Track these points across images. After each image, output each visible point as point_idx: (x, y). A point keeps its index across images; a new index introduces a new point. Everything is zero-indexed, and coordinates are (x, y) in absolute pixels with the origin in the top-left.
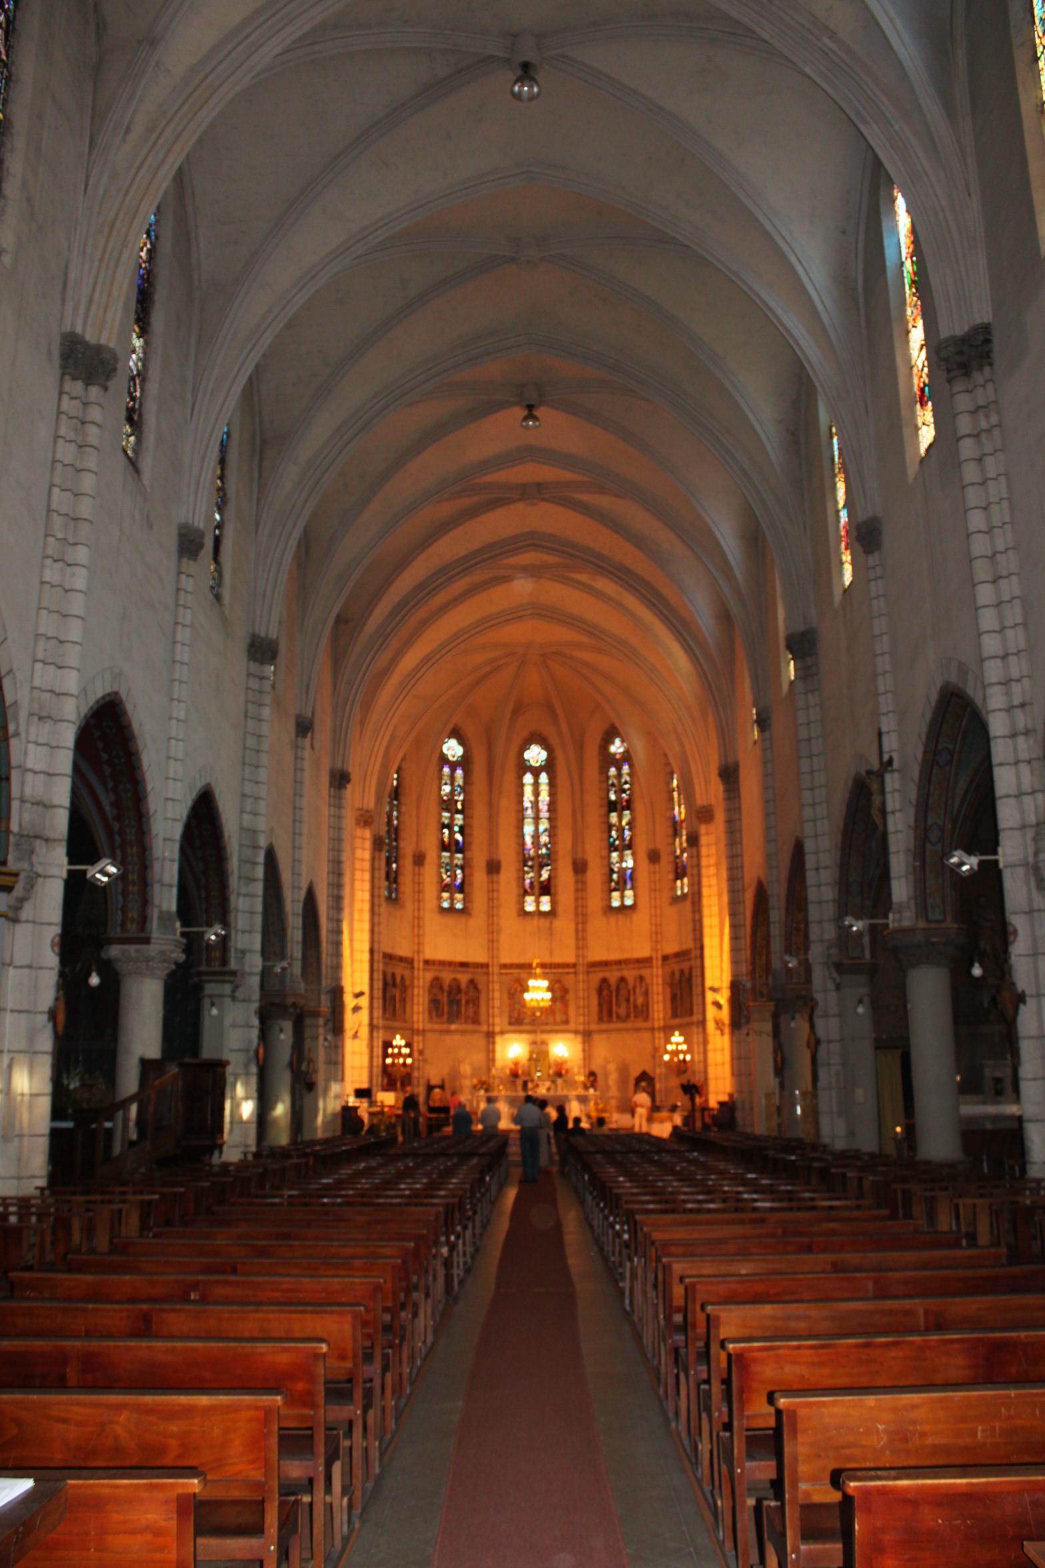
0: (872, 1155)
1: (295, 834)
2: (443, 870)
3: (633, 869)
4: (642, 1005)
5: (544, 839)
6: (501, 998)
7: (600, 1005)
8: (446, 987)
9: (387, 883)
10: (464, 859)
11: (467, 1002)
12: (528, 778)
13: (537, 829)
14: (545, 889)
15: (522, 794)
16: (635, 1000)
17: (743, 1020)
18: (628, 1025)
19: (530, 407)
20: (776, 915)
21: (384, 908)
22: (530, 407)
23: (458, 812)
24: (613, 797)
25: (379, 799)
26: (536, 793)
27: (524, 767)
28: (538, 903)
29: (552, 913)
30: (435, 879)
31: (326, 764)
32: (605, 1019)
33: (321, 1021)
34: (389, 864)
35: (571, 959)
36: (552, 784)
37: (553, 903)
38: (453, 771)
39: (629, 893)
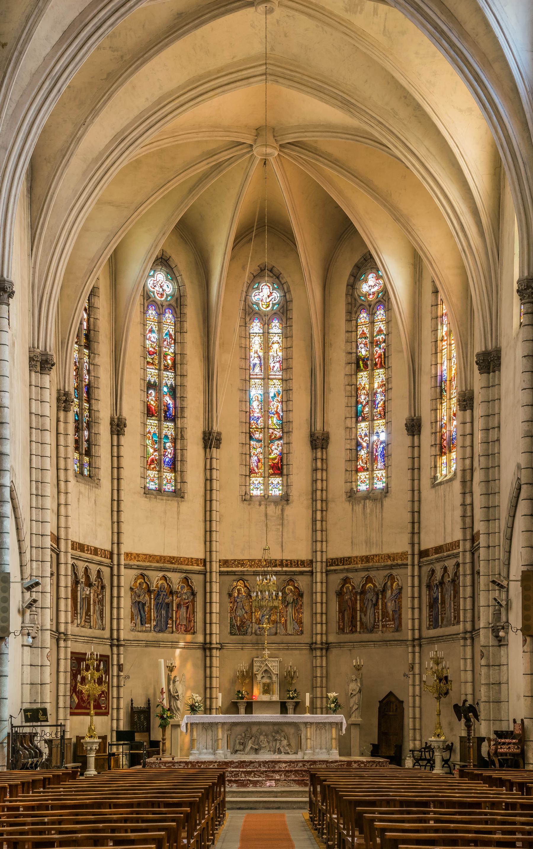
2: (149, 442)
3: (387, 444)
4: (164, 314)
5: (275, 405)
6: (220, 603)
7: (341, 611)
9: (77, 455)
10: (176, 428)
11: (179, 606)
12: (256, 327)
14: (278, 469)
18: (376, 636)
21: (73, 486)
23: (166, 368)
24: (363, 352)
26: (266, 346)
27: (250, 312)
28: (266, 485)
29: (286, 499)
30: (138, 452)
32: (347, 630)
35: (304, 554)
36: (287, 335)
37: (287, 486)
38: (160, 315)
39: (380, 473)
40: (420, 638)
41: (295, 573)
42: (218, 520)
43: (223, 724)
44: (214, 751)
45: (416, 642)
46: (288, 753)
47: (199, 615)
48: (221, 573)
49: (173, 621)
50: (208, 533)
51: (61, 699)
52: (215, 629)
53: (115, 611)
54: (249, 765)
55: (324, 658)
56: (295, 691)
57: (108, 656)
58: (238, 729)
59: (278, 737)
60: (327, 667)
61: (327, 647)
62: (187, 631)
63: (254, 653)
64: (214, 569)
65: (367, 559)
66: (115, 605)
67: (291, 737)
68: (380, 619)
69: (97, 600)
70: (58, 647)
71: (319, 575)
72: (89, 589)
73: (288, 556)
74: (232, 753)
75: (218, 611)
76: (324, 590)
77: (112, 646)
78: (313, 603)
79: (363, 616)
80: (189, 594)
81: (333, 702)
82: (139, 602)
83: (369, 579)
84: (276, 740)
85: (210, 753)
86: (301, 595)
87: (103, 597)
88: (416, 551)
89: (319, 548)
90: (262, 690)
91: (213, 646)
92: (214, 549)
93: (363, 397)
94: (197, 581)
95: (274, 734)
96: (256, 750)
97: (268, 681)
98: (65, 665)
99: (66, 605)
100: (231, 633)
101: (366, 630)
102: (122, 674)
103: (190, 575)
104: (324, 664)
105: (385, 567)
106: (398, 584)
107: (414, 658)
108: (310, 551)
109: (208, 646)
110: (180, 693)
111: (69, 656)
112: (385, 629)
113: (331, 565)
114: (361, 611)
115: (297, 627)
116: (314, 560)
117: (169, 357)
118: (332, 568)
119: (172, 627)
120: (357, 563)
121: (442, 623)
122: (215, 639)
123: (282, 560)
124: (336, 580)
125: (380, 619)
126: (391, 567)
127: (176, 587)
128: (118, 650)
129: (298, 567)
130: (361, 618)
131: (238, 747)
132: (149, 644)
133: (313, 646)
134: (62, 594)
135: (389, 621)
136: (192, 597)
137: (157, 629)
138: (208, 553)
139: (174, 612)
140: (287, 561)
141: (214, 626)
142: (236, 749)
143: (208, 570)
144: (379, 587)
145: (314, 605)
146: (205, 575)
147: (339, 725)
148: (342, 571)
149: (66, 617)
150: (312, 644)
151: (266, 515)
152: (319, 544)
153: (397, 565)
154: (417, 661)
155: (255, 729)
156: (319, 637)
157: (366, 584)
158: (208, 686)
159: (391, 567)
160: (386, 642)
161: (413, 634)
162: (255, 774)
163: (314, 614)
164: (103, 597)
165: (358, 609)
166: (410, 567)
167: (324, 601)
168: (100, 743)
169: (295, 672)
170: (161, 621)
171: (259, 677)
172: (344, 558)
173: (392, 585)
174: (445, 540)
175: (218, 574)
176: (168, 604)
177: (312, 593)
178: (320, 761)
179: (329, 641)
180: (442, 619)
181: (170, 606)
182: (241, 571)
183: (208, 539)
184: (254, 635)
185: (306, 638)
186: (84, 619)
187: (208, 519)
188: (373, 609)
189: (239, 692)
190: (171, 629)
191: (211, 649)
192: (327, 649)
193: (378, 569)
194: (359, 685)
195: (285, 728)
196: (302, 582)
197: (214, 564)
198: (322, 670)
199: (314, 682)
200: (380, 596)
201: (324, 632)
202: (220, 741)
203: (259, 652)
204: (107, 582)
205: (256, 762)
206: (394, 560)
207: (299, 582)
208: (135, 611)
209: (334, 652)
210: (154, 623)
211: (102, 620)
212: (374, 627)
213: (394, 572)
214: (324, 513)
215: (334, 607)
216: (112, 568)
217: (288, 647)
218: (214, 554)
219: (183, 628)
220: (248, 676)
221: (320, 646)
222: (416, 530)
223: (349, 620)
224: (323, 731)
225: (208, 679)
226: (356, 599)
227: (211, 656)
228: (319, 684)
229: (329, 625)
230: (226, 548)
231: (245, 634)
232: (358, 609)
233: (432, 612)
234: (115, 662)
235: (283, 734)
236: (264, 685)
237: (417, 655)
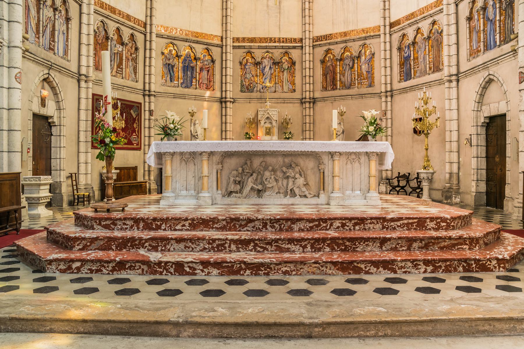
7: (325, 75)
11: (201, 69)
18: (353, 91)
35: (297, 35)
40: (391, 91)
41: (289, 48)
42: (232, 8)
43: (211, 154)
44: (198, 193)
45: (389, 94)
46: (305, 196)
47: (217, 77)
48: (234, 47)
49: (196, 80)
50: (224, 17)
51: (82, 134)
52: (229, 87)
53: (147, 68)
54: (246, 225)
55: (312, 109)
56: (290, 133)
57: (140, 104)
58: (233, 162)
59: (290, 173)
60: (313, 116)
61: (314, 101)
62: (207, 88)
63: (259, 105)
64: (228, 43)
65: (345, 34)
66: (147, 63)
67: (309, 172)
68: (356, 78)
69: (130, 58)
70: (79, 87)
71: (307, 48)
72: (121, 47)
73: (283, 35)
74: (224, 196)
75: (231, 74)
76: (311, 59)
77: (144, 95)
78: (303, 69)
79: (342, 77)
80: (209, 61)
81: (371, 124)
82: (169, 64)
83: (345, 49)
84: (288, 177)
85: (191, 196)
86: (294, 63)
87: (136, 56)
88: (387, 23)
89: (307, 29)
90: (264, 132)
91: (227, 100)
92: (229, 28)
94: (216, 52)
95: (284, 169)
96: (259, 191)
97: (269, 126)
98: (86, 104)
99: (88, 51)
100: (241, 91)
101: (344, 88)
102: (152, 118)
103: (210, 47)
104: (312, 114)
105: (360, 39)
106: (371, 51)
107: (386, 106)
108: (300, 32)
109: (224, 100)
110: (199, 133)
111: (90, 96)
112: (360, 85)
113: (316, 42)
115: (291, 87)
116: (304, 38)
118: (317, 43)
119: (196, 85)
120: (337, 38)
121: (414, 75)
122: (229, 95)
123: (280, 38)
124: (320, 52)
125: (356, 78)
126: (365, 38)
127: (199, 55)
128: (150, 99)
129: (292, 43)
130: (340, 79)
131: (232, 187)
132: (175, 96)
133: (303, 100)
134: (84, 40)
135: (364, 79)
136: (212, 64)
137: (184, 85)
138: (224, 32)
139: (198, 74)
140: (283, 38)
141: (228, 85)
142: (229, 190)
143: (224, 44)
144: (355, 54)
145: (304, 70)
146: (222, 48)
147: (381, 157)
148: (325, 45)
149: (88, 61)
150: (302, 99)
151: (268, 6)
152: (307, 25)
153: (370, 36)
154: (389, 108)
155: (257, 162)
156: (308, 93)
157: (344, 53)
158: (224, 129)
159: (365, 38)
160: (362, 96)
161: (386, 88)
162: (256, 245)
163: (304, 77)
164: (136, 56)
165: (338, 72)
166: (382, 36)
167: (311, 67)
168: (118, 173)
169: (289, 120)
170: (187, 79)
171: (262, 122)
172: (326, 35)
173: (365, 52)
174: (418, 5)
175: (232, 47)
176: (193, 68)
177: (302, 62)
178: (371, 218)
179: (315, 97)
180: (415, 72)
181: (194, 69)
182: (249, 46)
183: (224, 22)
184: (258, 93)
185: (297, 95)
186: (115, 70)
187: (224, 7)
188: (350, 71)
189: (247, 133)
190: (195, 87)
191: (226, 102)
192: (314, 103)
193: (354, 40)
194: (342, 127)
195: (301, 161)
196: (295, 54)
197: (228, 39)
198: (310, 118)
199: (304, 127)
200: (356, 61)
201: (311, 90)
202: (206, 179)
203: (262, 105)
204: (140, 44)
205: (258, 220)
206: (367, 32)
207: (292, 54)
208: (166, 71)
209: (319, 105)
210: (181, 81)
211: (135, 74)
212: (351, 85)
213: (368, 42)
214: (311, 3)
215: (319, 71)
216: (145, 35)
217: (284, 101)
218: (229, 32)
219: (205, 86)
220: (255, 122)
221: (309, 100)
222: (387, 7)
223: (330, 80)
224: (357, 165)
225: (224, 125)
226: (336, 65)
227: (226, 107)
228: (308, 129)
229: (315, 85)
230: (239, 28)
231: (252, 91)
232: (338, 72)
233: (402, 68)
234: (147, 109)
235: (297, 169)
236: (266, 128)
237: (389, 104)
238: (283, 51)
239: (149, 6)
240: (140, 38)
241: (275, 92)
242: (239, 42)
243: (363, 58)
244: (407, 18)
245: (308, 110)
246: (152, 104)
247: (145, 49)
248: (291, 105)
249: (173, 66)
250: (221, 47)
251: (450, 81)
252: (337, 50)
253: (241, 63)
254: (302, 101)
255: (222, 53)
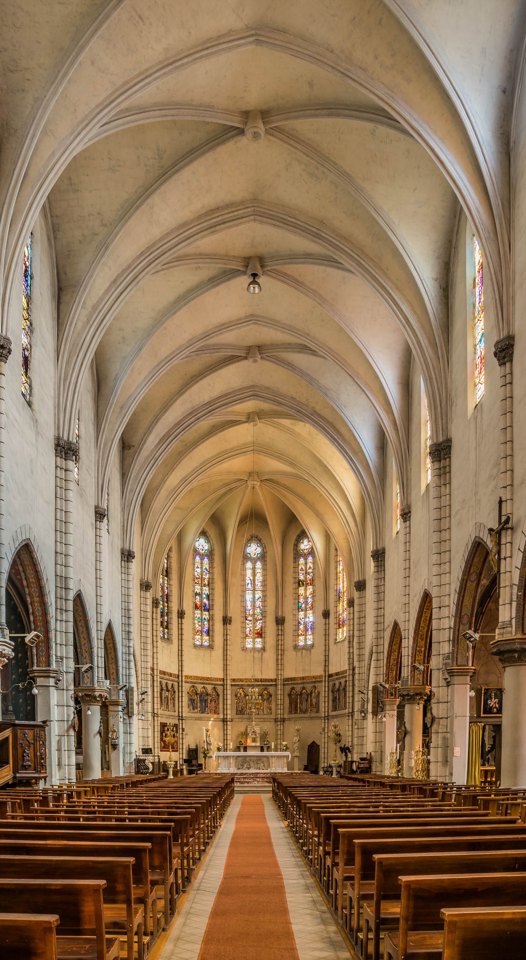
0: (273, 793)
1: (97, 586)
2: (196, 622)
4: (204, 559)
5: (258, 603)
7: (290, 703)
8: (199, 692)
10: (209, 615)
11: (211, 701)
13: (254, 597)
15: (244, 576)
16: (311, 700)
17: (379, 710)
19: (254, 275)
20: (408, 644)
22: (254, 275)
23: (205, 585)
25: (155, 575)
26: (254, 575)
27: (246, 558)
28: (254, 643)
29: (263, 649)
30: (191, 627)
31: (118, 545)
33: (120, 708)
34: (162, 616)
35: (272, 676)
36: (264, 569)
37: (264, 643)
38: (202, 559)
41: (268, 685)
43: (233, 756)
47: (221, 705)
48: (232, 685)
51: (156, 744)
52: (229, 712)
58: (240, 759)
59: (259, 762)
61: (283, 720)
64: (228, 683)
65: (303, 678)
66: (180, 700)
71: (279, 686)
73: (264, 677)
77: (179, 720)
78: (276, 699)
83: (304, 688)
86: (271, 696)
88: (327, 675)
89: (279, 673)
93: (302, 599)
94: (220, 689)
97: (255, 736)
98: (158, 728)
100: (237, 714)
105: (312, 682)
107: (325, 725)
108: (275, 675)
110: (212, 742)
111: (159, 724)
114: (300, 703)
115: (269, 711)
117: (206, 580)
124: (288, 688)
126: (315, 682)
131: (240, 767)
134: (156, 696)
144: (309, 692)
146: (224, 686)
147: (287, 757)
148: (291, 684)
149: (157, 706)
153: (318, 681)
154: (326, 726)
155: (248, 759)
156: (279, 716)
160: (312, 718)
161: (325, 714)
163: (277, 705)
166: (324, 682)
171: (250, 735)
176: (206, 700)
185: (273, 716)
191: (227, 721)
192: (283, 721)
193: (308, 683)
196: (271, 690)
197: (228, 681)
208: (190, 703)
209: (287, 723)
215: (287, 701)
216: (178, 683)
217: (265, 720)
218: (228, 676)
220: (245, 734)
223: (294, 708)
227: (227, 725)
230: (234, 673)
231: (244, 714)
234: (181, 727)
236: (253, 738)
237: (326, 724)
238: (264, 687)
239: (180, 665)
240: (176, 684)
241: (258, 714)
242: (381, 782)
243: (313, 695)
244: (337, 674)
245: (279, 726)
246: (184, 725)
247: (179, 692)
248: (269, 723)
249: (194, 700)
250: (223, 685)
251: (349, 716)
252: (298, 688)
253: (236, 696)
254: (276, 720)
255: (224, 690)
